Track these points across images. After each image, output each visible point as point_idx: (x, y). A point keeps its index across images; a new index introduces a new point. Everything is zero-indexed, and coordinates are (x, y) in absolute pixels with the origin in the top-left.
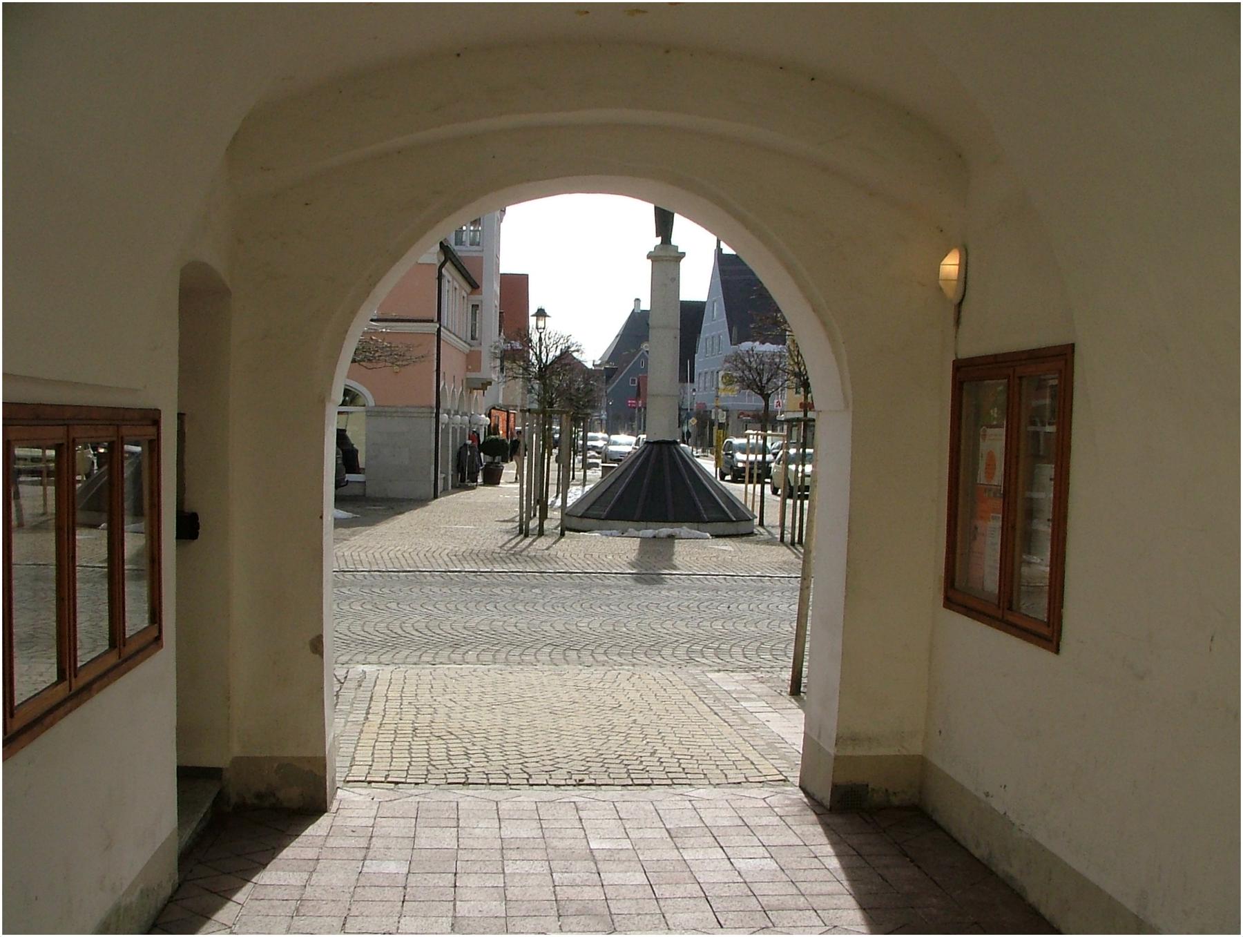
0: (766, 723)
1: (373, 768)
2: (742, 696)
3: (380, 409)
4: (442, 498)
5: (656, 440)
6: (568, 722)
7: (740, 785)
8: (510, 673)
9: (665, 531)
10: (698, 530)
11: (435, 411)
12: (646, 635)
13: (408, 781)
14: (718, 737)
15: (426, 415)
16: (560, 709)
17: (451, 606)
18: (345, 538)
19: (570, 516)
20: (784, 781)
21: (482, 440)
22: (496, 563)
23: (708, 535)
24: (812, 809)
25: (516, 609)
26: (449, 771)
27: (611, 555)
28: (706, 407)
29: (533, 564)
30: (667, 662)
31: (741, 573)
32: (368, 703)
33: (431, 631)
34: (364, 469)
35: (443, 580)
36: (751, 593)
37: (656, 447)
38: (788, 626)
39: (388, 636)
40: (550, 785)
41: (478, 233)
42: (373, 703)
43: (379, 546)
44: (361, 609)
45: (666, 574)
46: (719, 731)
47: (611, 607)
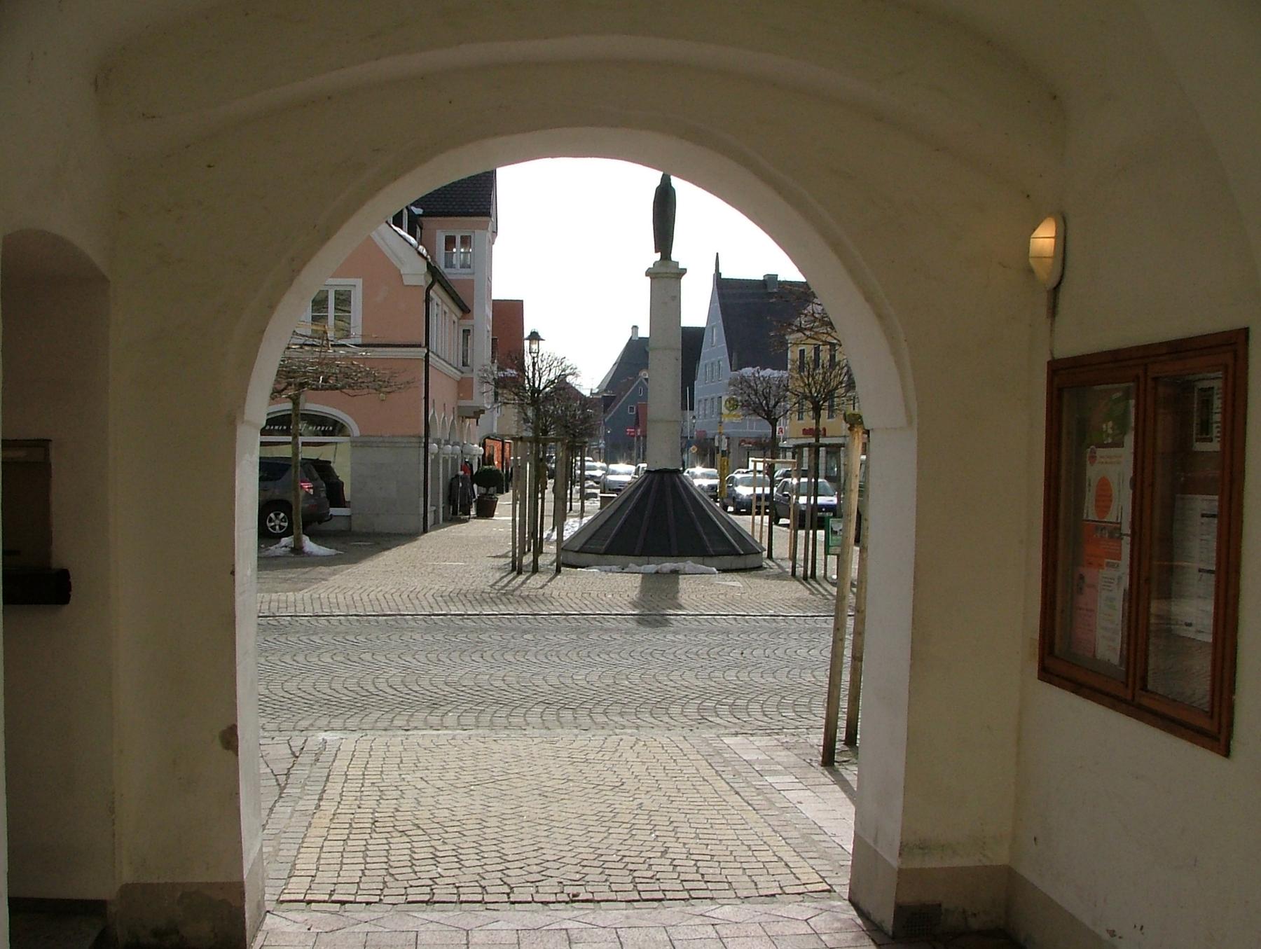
0: (798, 805)
1: (317, 880)
2: (767, 767)
3: (366, 439)
4: (433, 533)
5: (657, 468)
6: (561, 808)
7: (775, 899)
8: (495, 740)
9: (668, 565)
10: (703, 564)
11: (424, 441)
12: (650, 690)
13: (359, 899)
14: (742, 827)
15: (413, 445)
16: (550, 789)
17: (432, 656)
18: (324, 577)
19: (566, 550)
20: (829, 891)
21: (475, 470)
22: (485, 604)
23: (715, 569)
24: (869, 936)
25: (504, 659)
26: (410, 883)
27: (611, 593)
28: (706, 434)
29: (526, 605)
30: (676, 723)
31: (753, 612)
32: (323, 784)
33: (407, 687)
34: (349, 502)
35: (427, 625)
36: (765, 636)
37: (657, 477)
38: (810, 675)
39: (357, 694)
40: (536, 902)
41: (469, 255)
42: (329, 784)
43: (359, 587)
44: (331, 661)
45: (670, 615)
46: (742, 818)
47: (611, 655)
